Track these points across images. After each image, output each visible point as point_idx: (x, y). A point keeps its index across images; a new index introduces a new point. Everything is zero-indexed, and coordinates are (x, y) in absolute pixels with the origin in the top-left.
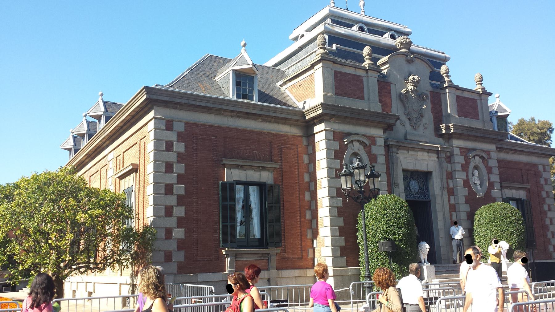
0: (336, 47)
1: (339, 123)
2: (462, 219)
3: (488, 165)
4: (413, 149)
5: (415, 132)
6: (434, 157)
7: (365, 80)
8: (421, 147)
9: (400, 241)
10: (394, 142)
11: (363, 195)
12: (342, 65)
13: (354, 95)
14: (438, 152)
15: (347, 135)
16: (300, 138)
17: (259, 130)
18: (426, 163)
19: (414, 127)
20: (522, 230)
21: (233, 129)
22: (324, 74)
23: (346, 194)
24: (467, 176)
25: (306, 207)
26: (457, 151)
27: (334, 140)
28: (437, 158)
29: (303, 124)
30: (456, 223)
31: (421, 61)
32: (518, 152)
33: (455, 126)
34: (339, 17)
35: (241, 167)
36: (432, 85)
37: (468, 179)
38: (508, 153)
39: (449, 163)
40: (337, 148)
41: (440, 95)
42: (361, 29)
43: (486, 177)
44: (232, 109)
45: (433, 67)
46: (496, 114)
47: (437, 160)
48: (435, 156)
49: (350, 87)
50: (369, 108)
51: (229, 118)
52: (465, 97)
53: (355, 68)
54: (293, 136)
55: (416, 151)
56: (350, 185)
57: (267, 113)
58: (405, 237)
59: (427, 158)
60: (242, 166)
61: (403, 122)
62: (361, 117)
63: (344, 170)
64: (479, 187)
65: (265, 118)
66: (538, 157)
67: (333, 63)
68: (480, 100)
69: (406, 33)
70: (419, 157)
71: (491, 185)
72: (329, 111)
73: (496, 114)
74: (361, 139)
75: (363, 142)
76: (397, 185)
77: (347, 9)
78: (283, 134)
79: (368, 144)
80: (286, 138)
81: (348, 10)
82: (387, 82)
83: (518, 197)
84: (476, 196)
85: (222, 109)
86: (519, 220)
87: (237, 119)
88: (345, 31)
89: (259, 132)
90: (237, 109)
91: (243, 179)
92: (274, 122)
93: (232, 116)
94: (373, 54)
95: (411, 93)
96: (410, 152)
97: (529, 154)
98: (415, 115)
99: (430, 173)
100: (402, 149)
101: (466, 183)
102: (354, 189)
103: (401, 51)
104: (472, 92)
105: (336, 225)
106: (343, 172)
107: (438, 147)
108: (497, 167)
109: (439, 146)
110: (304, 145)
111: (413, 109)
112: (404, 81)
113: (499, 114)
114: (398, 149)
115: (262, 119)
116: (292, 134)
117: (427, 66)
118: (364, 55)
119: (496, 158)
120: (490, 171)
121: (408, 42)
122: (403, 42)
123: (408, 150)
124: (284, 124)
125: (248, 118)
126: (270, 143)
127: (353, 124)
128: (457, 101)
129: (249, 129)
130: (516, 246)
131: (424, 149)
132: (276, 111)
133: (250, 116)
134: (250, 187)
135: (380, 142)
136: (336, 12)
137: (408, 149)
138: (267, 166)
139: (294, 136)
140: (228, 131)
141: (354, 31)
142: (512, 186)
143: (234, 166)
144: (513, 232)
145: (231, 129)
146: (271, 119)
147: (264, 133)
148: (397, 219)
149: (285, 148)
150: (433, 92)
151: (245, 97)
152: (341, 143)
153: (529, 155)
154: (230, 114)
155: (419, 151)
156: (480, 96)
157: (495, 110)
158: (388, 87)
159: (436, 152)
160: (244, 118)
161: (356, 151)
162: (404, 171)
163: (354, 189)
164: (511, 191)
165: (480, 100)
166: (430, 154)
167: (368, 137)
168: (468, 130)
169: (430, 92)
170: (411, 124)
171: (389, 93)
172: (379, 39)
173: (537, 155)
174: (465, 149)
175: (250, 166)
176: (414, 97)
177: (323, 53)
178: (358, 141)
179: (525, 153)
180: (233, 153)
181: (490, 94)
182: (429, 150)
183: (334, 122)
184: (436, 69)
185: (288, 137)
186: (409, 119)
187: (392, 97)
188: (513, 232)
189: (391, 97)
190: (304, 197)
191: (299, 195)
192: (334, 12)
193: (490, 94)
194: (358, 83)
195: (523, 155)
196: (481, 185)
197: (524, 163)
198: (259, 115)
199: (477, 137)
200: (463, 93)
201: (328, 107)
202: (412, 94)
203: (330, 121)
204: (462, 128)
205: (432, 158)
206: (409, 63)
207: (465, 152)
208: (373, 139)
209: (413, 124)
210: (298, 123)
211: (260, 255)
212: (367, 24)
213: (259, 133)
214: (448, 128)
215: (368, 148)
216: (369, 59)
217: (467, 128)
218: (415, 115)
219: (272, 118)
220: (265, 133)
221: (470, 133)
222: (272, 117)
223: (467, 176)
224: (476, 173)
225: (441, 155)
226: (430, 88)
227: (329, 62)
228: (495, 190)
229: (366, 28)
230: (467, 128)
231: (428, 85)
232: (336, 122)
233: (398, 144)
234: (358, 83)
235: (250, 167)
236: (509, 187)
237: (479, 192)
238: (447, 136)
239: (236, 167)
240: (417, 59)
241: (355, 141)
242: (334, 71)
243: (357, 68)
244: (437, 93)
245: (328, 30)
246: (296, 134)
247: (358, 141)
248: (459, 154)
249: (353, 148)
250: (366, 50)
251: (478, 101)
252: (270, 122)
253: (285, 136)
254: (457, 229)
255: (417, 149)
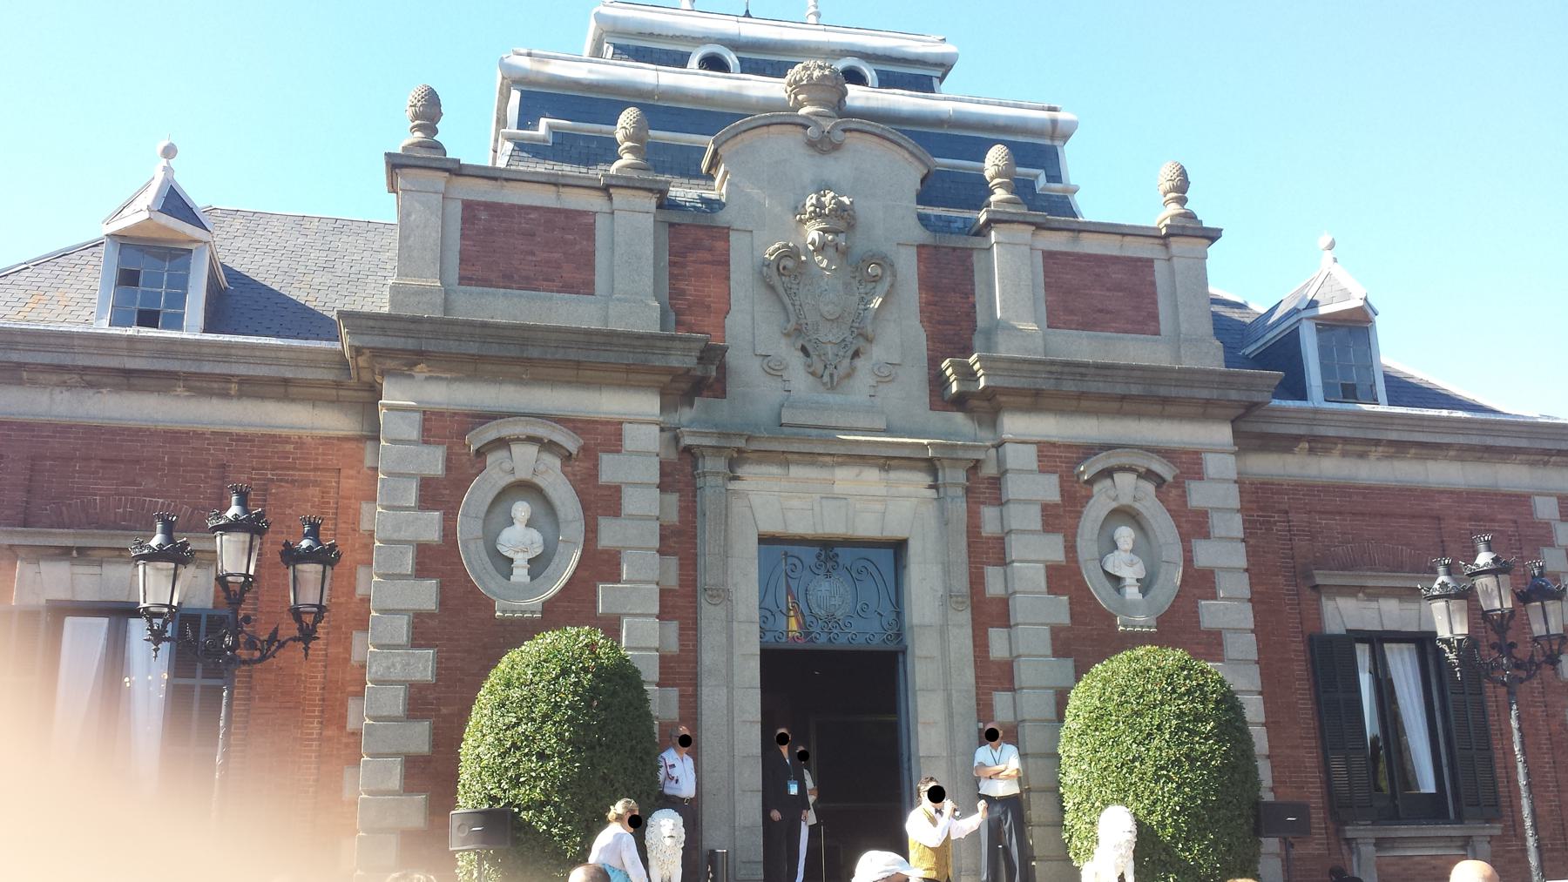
0: (550, 127)
1: (450, 381)
2: (1027, 717)
3: (1185, 503)
4: (810, 458)
5: (830, 398)
6: (915, 484)
7: (601, 224)
8: (843, 450)
9: (539, 806)
10: (706, 435)
11: (1510, 656)
12: (495, 179)
13: (544, 280)
14: (931, 466)
15: (1089, 450)
16: (353, 445)
17: (178, 427)
18: (878, 507)
19: (830, 378)
20: (1212, 759)
21: (71, 427)
22: (409, 215)
23: (1451, 656)
24: (1071, 549)
25: (351, 689)
26: (1020, 458)
27: (425, 442)
28: (931, 487)
29: (361, 394)
30: (991, 736)
31: (876, 139)
32: (1413, 451)
33: (988, 364)
34: (641, 35)
35: (80, 555)
36: (923, 220)
37: (1077, 562)
38: (1362, 456)
39: (993, 505)
40: (1054, 496)
41: (970, 256)
42: (714, 63)
43: (1174, 552)
44: (56, 362)
45: (927, 156)
46: (1310, 313)
47: (932, 493)
48: (923, 479)
49: (533, 254)
50: (606, 319)
51: (58, 390)
52: (1089, 256)
53: (555, 185)
54: (321, 438)
55: (824, 465)
56: (1461, 624)
57: (191, 367)
58: (561, 792)
59: (881, 490)
60: (82, 551)
61: (771, 364)
62: (535, 353)
63: (1440, 580)
64: (1132, 592)
65: (198, 384)
66: (1532, 464)
67: (447, 174)
68: (1169, 260)
69: (932, 60)
70: (839, 488)
71: (1199, 582)
72: (383, 339)
73: (1310, 313)
74: (542, 431)
75: (551, 442)
76: (722, 594)
77: (747, 15)
78: (280, 436)
79: (1169, 477)
80: (290, 448)
81: (750, 17)
82: (715, 227)
83: (1416, 630)
84: (1116, 627)
85: (20, 366)
86: (1199, 718)
87: (90, 392)
88: (590, 71)
89: (179, 432)
90: (67, 360)
91: (1373, 625)
92: (241, 395)
93: (64, 384)
94: (1019, 170)
95: (818, 258)
96: (795, 471)
97: (1479, 455)
98: (830, 335)
99: (898, 548)
100: (759, 462)
101: (1063, 578)
102: (1121, 628)
103: (802, 112)
104: (1124, 235)
105: (393, 750)
106: (1436, 586)
107: (922, 444)
108: (1238, 511)
109: (925, 442)
110: (369, 468)
111: (821, 315)
112: (791, 217)
113: (1322, 310)
114: (733, 464)
115: (189, 389)
116: (315, 432)
117: (907, 155)
118: (988, 175)
119: (1235, 477)
120: (1194, 526)
121: (819, 78)
122: (801, 80)
123: (786, 464)
124: (286, 398)
125: (131, 388)
126: (223, 466)
127: (519, 381)
128: (1047, 272)
129: (132, 424)
130: (1177, 827)
131: (858, 458)
132: (227, 355)
133: (134, 381)
134: (1386, 645)
135: (644, 440)
136: (626, 19)
137: (784, 459)
138: (88, 545)
139: (327, 441)
140: (48, 437)
141: (694, 80)
142: (1370, 583)
143: (51, 551)
144: (1162, 768)
145: (63, 430)
146: (223, 385)
147: (199, 435)
148: (533, 720)
149: (281, 480)
150: (936, 247)
151: (148, 318)
152: (457, 449)
153: (1480, 459)
154: (55, 378)
155: (841, 464)
156: (1166, 246)
157: (1309, 298)
158: (720, 245)
159: (923, 464)
160: (117, 388)
161: (1126, 500)
162: (766, 540)
163: (1121, 628)
164: (1374, 605)
165: (1169, 260)
166: (893, 475)
167: (1167, 454)
168: (1062, 373)
169: (921, 247)
170: (809, 366)
171: (723, 263)
172: (741, 87)
173: (1524, 457)
174: (1069, 447)
175: (114, 549)
176: (830, 270)
177: (1179, 215)
178: (531, 439)
179: (1452, 453)
180: (64, 508)
181: (1213, 236)
182: (887, 462)
183: (427, 379)
184: (937, 159)
185: (303, 443)
186: (804, 350)
187: (732, 276)
188: (1162, 768)
189: (728, 278)
190: (348, 650)
191: (327, 645)
192: (615, 19)
193: (1213, 236)
194: (571, 237)
195: (1445, 457)
196: (1145, 585)
197: (1452, 492)
198: (1518, 451)
199: (1123, 398)
200: (1076, 240)
201: (371, 323)
202: (822, 262)
203: (411, 376)
204: (1026, 367)
205: (905, 489)
206: (823, 152)
207: (1051, 455)
208: (1190, 463)
209: (819, 367)
210: (342, 393)
211: (1459, 844)
212: (735, 45)
213: (174, 437)
214: (967, 375)
215: (1170, 491)
216: (630, 150)
217: (1054, 369)
218: (830, 335)
219: (230, 382)
220: (203, 434)
221: (1069, 386)
222: (227, 378)
223: (1071, 549)
224: (1125, 535)
225: (944, 474)
226: (920, 235)
227: (547, 187)
228: (627, 582)
229: (732, 58)
230: (1054, 369)
231: (913, 221)
232: (441, 379)
233: (724, 443)
234: (571, 237)
235: (117, 553)
236: (1362, 588)
237: (1130, 608)
238: (985, 404)
239: (59, 555)
240: (848, 134)
241: (518, 440)
242: (463, 201)
243: (565, 185)
244: (954, 249)
245: (516, 76)
246: (332, 433)
247: (531, 439)
248: (1035, 466)
249: (1112, 493)
250: (994, 159)
251: (1158, 266)
252: (225, 395)
253: (286, 440)
254: (996, 755)
255: (828, 459)
